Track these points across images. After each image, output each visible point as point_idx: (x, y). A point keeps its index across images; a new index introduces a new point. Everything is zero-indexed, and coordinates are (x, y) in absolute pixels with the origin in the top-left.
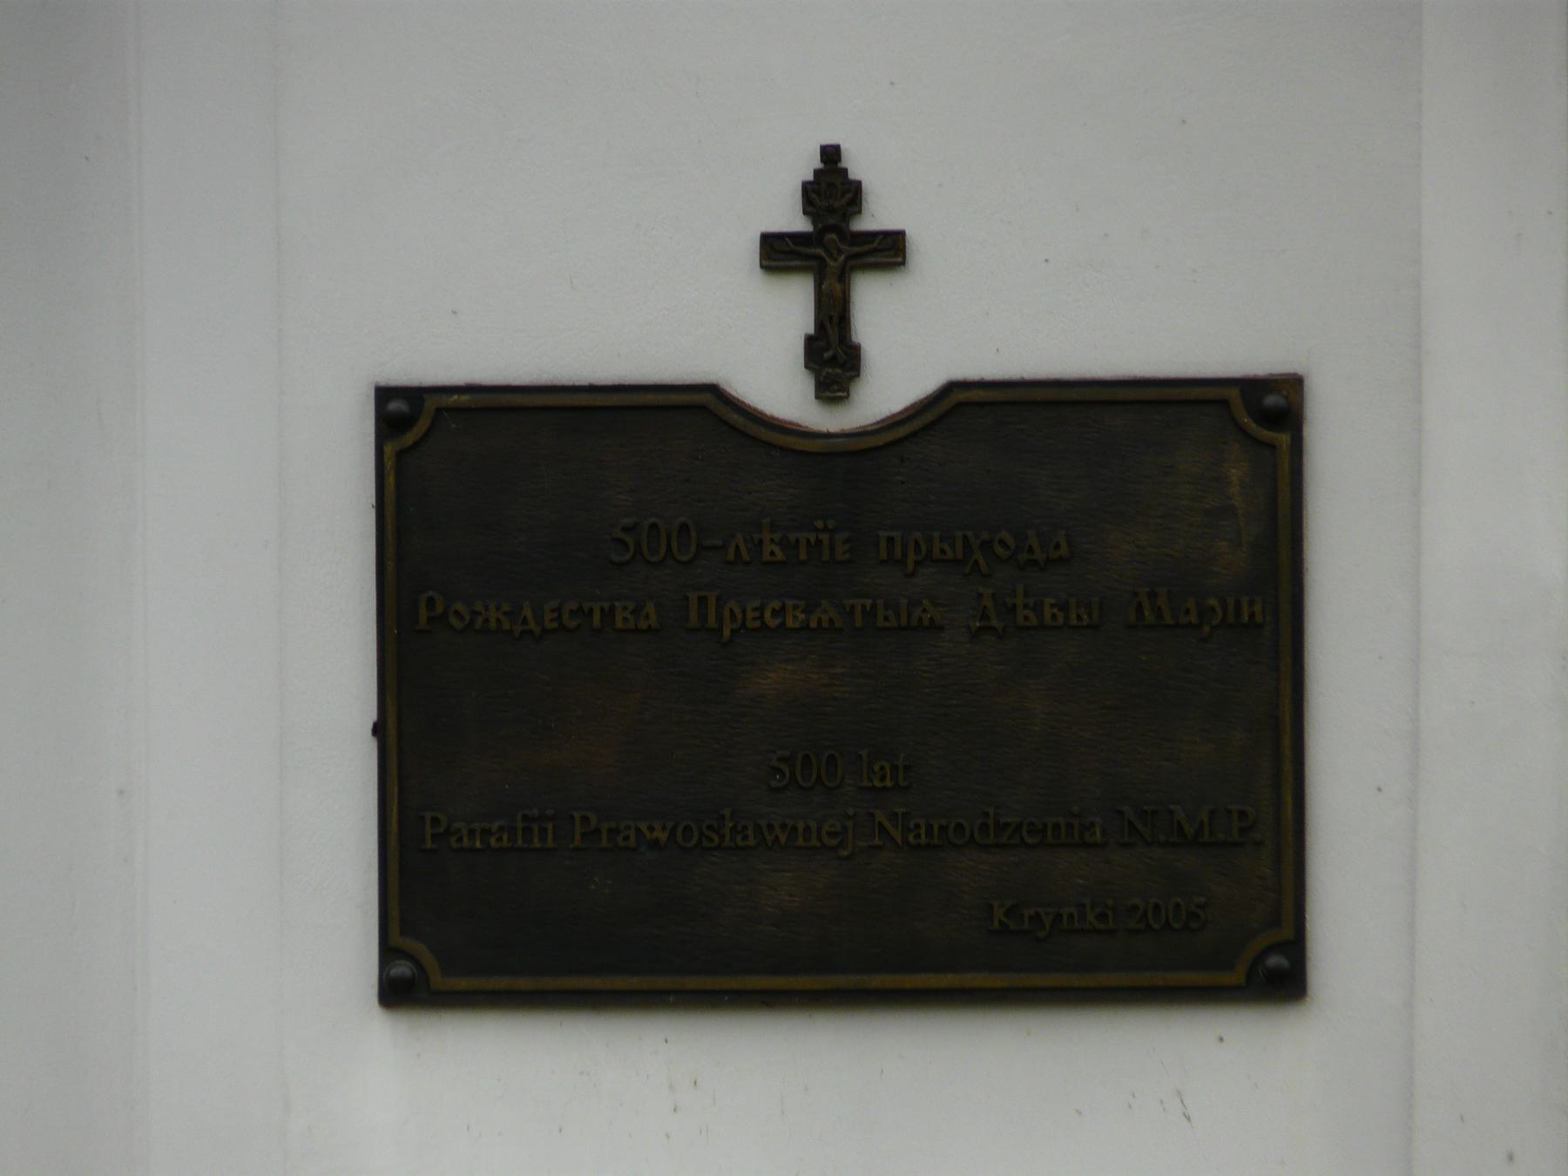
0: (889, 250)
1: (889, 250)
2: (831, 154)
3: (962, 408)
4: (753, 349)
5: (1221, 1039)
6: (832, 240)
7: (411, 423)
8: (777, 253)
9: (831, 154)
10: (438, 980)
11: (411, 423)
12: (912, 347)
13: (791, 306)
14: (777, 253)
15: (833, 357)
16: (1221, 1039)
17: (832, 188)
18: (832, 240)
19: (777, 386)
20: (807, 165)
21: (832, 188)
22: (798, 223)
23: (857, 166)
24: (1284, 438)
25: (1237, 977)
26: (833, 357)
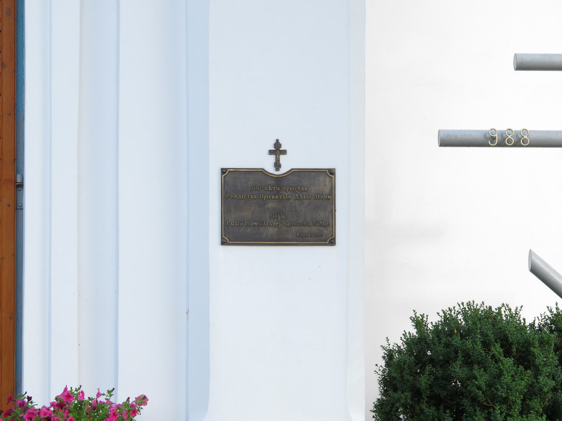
0: (284, 152)
1: (284, 152)
2: (277, 140)
3: (294, 172)
4: (267, 164)
5: (10, 114)
6: (277, 150)
7: (330, 240)
8: (271, 152)
9: (277, 140)
10: (228, 242)
11: (330, 240)
12: (288, 164)
13: (272, 158)
14: (271, 152)
15: (277, 165)
16: (10, 114)
17: (277, 144)
18: (277, 150)
19: (271, 169)
20: (274, 142)
21: (277, 144)
22: (274, 149)
23: (280, 142)
24: (333, 176)
25: (327, 242)
26: (277, 165)
